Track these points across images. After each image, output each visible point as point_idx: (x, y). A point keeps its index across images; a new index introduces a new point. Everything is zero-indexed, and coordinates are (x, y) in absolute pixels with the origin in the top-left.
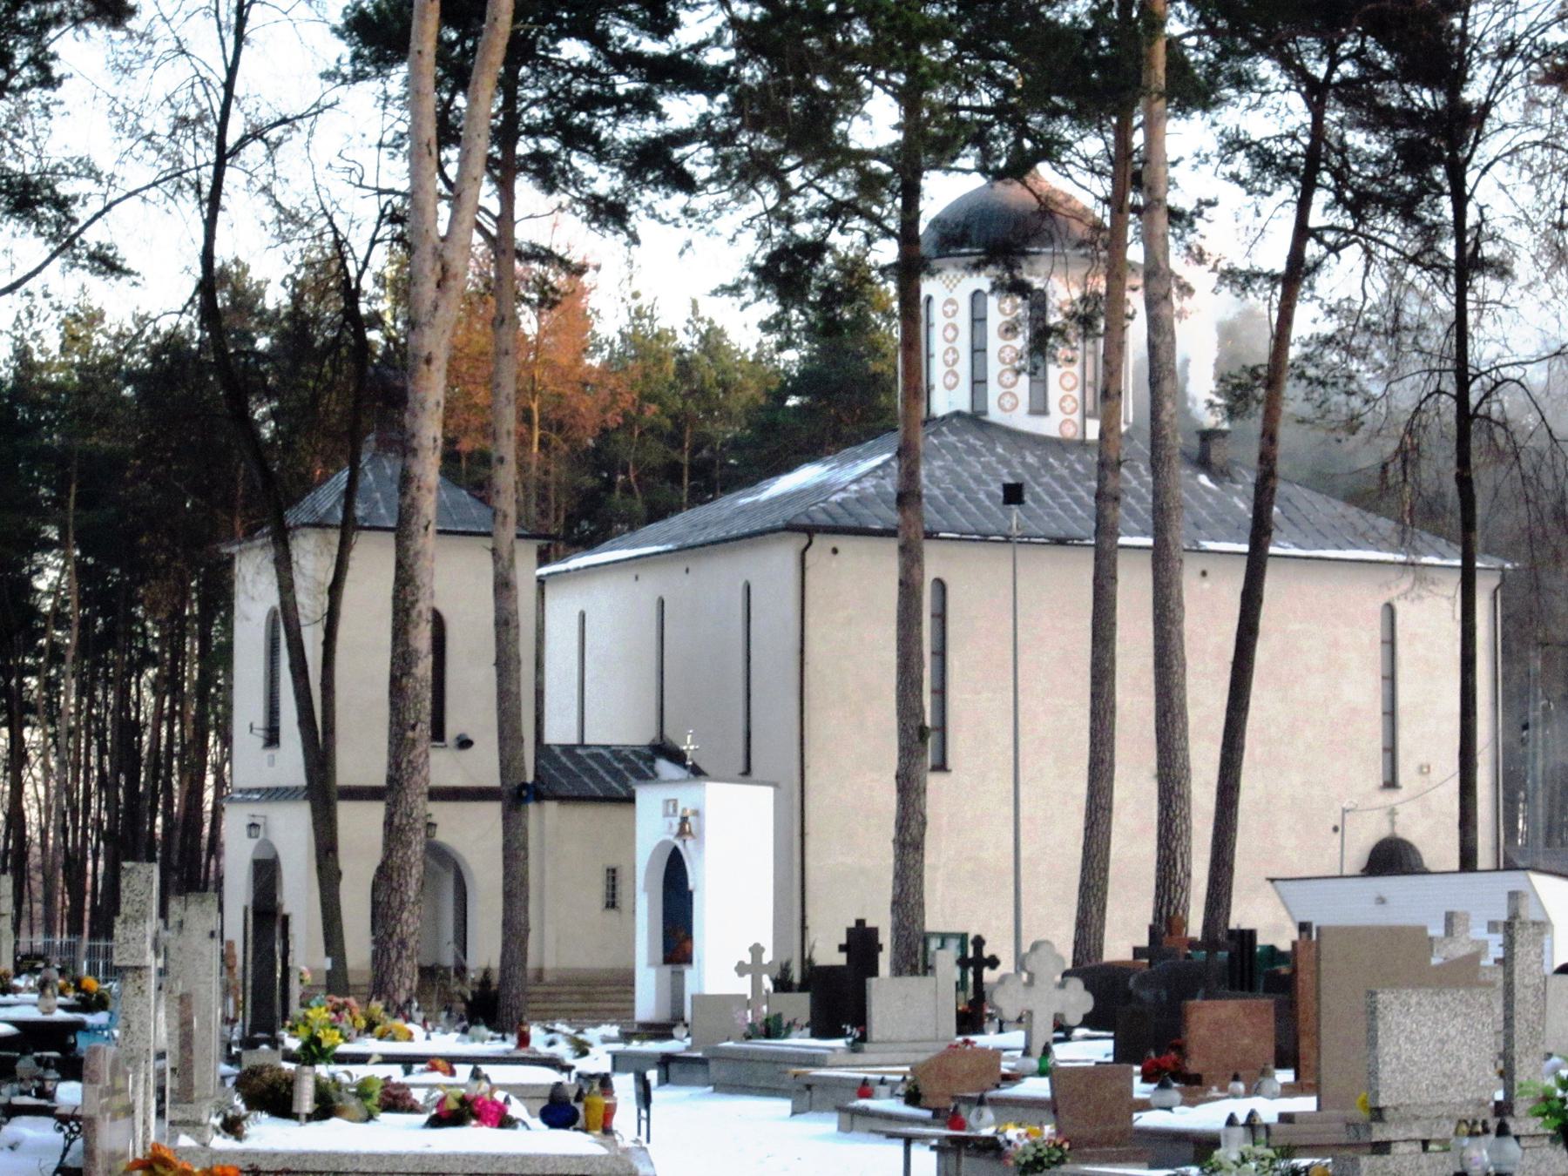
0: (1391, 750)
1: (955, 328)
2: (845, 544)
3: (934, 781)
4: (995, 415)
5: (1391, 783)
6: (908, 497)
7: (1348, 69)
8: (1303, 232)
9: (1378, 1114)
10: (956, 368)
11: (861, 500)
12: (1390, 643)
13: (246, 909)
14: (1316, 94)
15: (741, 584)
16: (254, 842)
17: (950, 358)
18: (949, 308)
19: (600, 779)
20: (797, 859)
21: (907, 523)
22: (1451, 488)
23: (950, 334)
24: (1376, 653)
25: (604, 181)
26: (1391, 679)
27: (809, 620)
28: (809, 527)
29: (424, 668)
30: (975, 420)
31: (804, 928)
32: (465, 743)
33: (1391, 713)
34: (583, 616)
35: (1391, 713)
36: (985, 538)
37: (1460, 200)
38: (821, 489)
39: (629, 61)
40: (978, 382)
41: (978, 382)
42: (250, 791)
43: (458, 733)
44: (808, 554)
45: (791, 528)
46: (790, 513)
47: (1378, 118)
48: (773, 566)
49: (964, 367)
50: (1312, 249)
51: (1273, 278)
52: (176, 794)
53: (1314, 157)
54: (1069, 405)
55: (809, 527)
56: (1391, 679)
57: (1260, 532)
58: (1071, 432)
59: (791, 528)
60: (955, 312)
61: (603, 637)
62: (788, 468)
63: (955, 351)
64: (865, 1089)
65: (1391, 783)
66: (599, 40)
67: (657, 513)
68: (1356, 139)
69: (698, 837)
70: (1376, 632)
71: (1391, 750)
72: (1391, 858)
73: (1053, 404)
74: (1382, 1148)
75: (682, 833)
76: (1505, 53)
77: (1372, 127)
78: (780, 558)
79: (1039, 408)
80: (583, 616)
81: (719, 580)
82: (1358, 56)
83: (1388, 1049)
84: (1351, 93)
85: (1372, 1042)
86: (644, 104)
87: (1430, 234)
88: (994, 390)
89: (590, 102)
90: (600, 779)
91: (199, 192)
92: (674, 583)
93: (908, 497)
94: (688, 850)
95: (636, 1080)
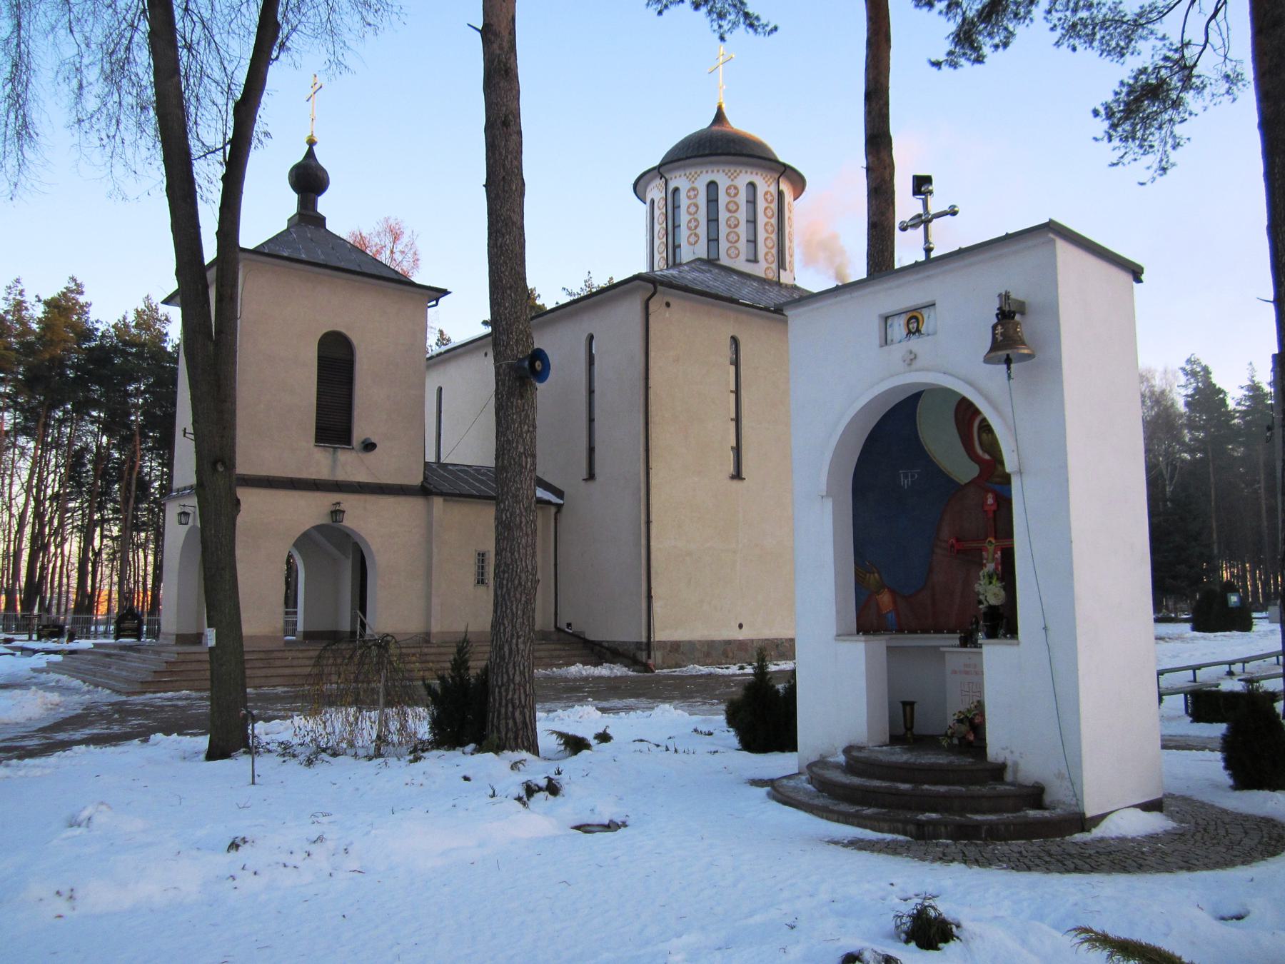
1: (696, 206)
4: (724, 260)
10: (698, 231)
13: (482, 556)
15: (584, 337)
16: (186, 528)
17: (693, 225)
18: (692, 193)
20: (643, 541)
23: (693, 209)
27: (652, 354)
31: (649, 597)
32: (369, 446)
34: (440, 390)
40: (713, 240)
41: (713, 240)
42: (185, 489)
43: (363, 438)
44: (650, 302)
49: (702, 230)
52: (933, 788)
54: (770, 258)
60: (696, 196)
63: (696, 220)
73: (761, 256)
80: (440, 390)
88: (723, 245)
95: (234, 466)
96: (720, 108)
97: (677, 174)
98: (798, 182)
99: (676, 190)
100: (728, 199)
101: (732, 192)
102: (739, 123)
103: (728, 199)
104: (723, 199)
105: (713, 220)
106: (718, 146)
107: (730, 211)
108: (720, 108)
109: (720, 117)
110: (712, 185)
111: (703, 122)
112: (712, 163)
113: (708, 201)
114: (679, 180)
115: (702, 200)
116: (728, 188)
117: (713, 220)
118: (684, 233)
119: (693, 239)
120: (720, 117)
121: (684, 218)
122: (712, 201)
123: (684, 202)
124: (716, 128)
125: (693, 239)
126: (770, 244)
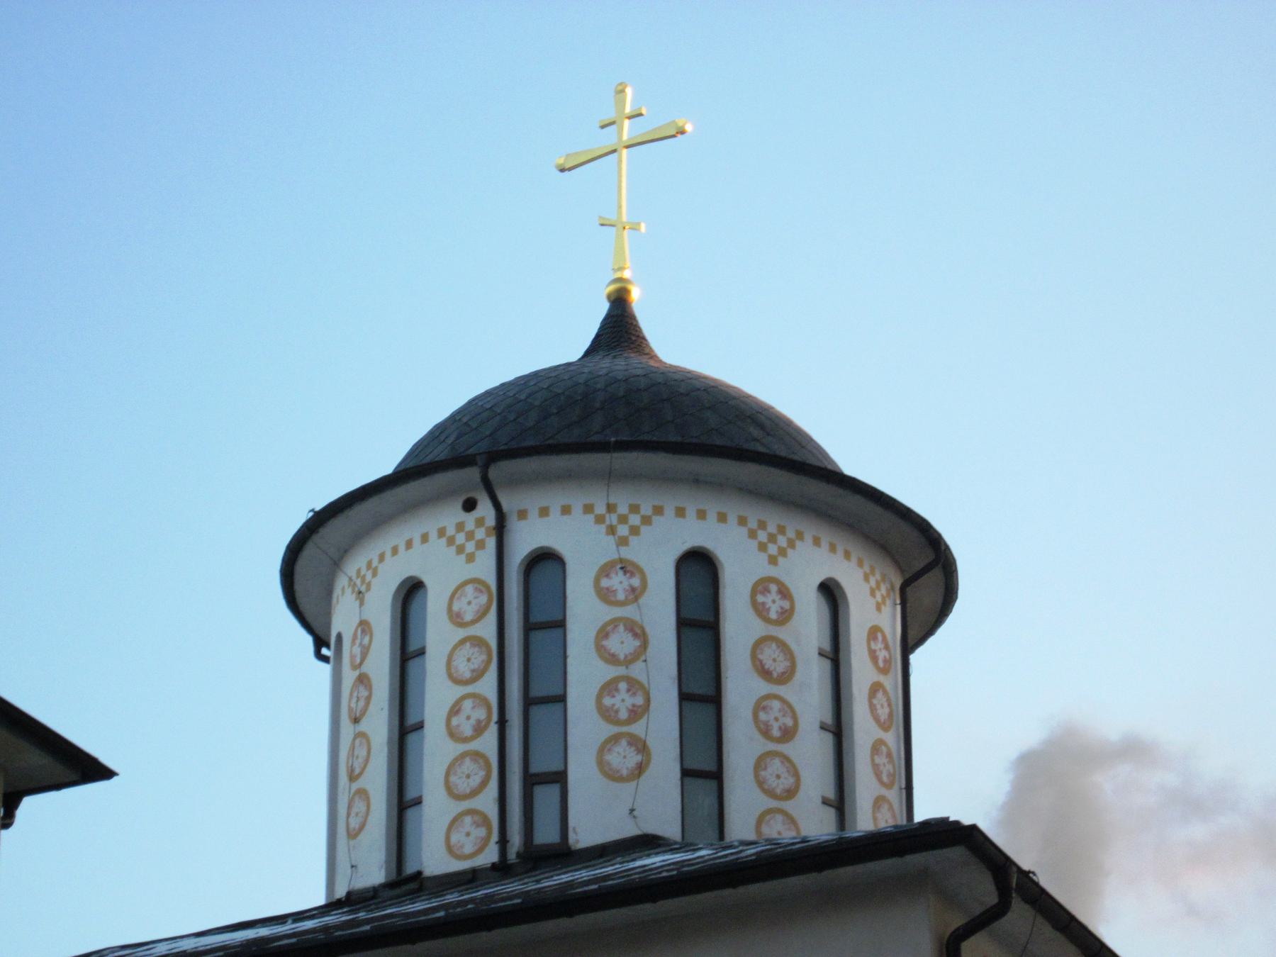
18: (618, 582)
23: (621, 643)
49: (663, 724)
96: (619, 305)
97: (554, 498)
98: (924, 572)
99: (545, 561)
100: (759, 629)
101: (774, 604)
102: (681, 341)
103: (759, 629)
104: (739, 627)
105: (702, 696)
106: (617, 415)
107: (765, 674)
108: (619, 305)
109: (619, 328)
110: (698, 568)
111: (565, 340)
112: (697, 481)
113: (684, 623)
114: (566, 522)
115: (660, 610)
116: (761, 586)
117: (702, 696)
118: (585, 727)
119: (623, 758)
120: (619, 328)
121: (585, 673)
122: (699, 624)
123: (584, 611)
124: (604, 364)
125: (623, 758)
126: (473, 713)
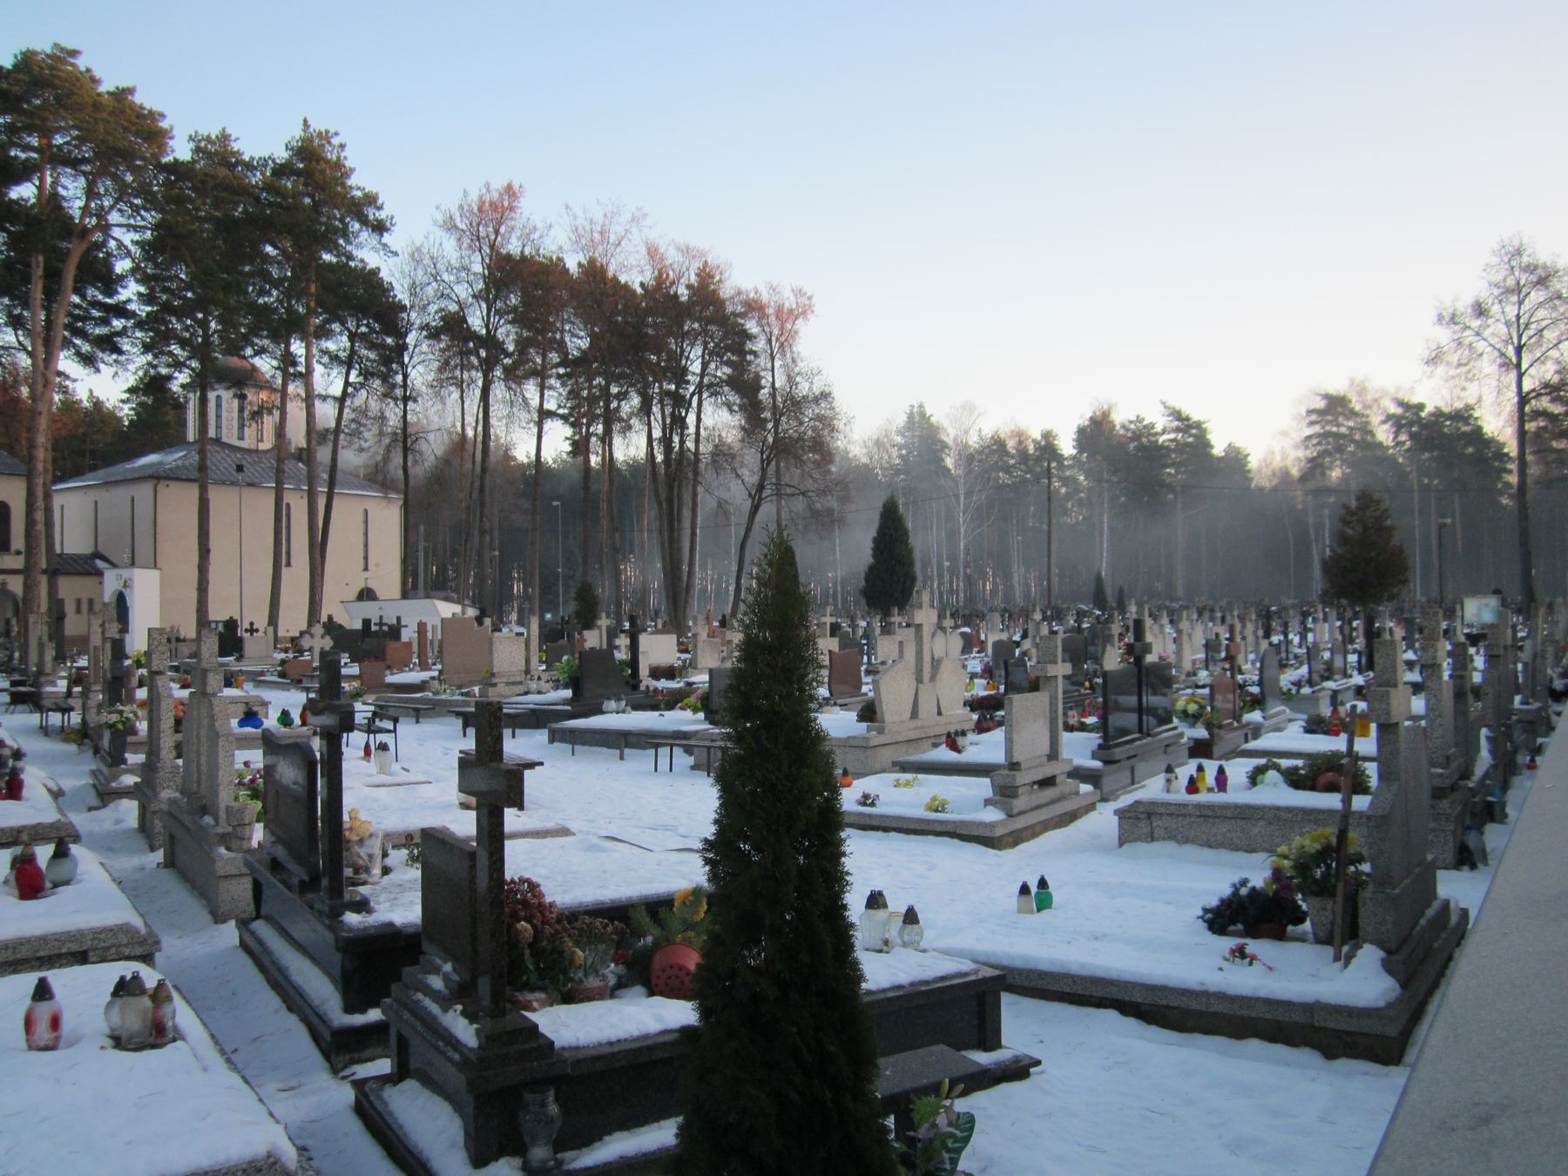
0: (366, 558)
2: (172, 484)
3: (284, 570)
4: (224, 439)
5: (366, 569)
6: (202, 467)
7: (363, 329)
8: (347, 384)
9: (493, 675)
11: (177, 467)
12: (366, 522)
14: (353, 337)
19: (87, 566)
21: (201, 477)
22: (400, 473)
24: (362, 526)
25: (86, 348)
26: (366, 534)
28: (158, 477)
29: (41, 527)
30: (217, 441)
33: (366, 546)
35: (366, 546)
36: (224, 483)
37: (405, 376)
38: (160, 463)
39: (95, 304)
45: (151, 477)
46: (149, 472)
47: (372, 346)
48: (144, 491)
50: (350, 390)
51: (335, 398)
53: (350, 357)
55: (158, 477)
56: (366, 534)
57: (279, 483)
58: (253, 447)
59: (151, 477)
61: (76, 513)
62: (144, 454)
64: (262, 673)
65: (366, 569)
66: (83, 297)
67: (94, 468)
68: (364, 352)
69: (131, 587)
70: (362, 518)
71: (366, 558)
72: (367, 595)
74: (494, 685)
75: (125, 586)
76: (422, 328)
77: (369, 349)
78: (146, 489)
79: (241, 438)
81: (121, 495)
82: (367, 325)
83: (495, 655)
84: (363, 337)
85: (491, 653)
86: (105, 322)
87: (394, 386)
88: (224, 430)
89: (84, 319)
90: (87, 566)
91: (25, 349)
92: (102, 496)
93: (202, 467)
94: (127, 593)
